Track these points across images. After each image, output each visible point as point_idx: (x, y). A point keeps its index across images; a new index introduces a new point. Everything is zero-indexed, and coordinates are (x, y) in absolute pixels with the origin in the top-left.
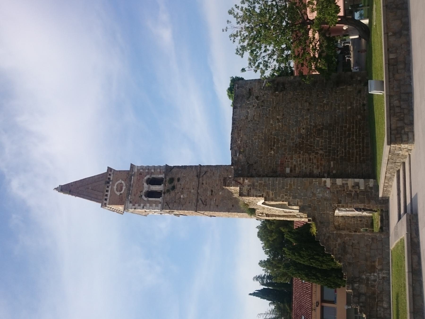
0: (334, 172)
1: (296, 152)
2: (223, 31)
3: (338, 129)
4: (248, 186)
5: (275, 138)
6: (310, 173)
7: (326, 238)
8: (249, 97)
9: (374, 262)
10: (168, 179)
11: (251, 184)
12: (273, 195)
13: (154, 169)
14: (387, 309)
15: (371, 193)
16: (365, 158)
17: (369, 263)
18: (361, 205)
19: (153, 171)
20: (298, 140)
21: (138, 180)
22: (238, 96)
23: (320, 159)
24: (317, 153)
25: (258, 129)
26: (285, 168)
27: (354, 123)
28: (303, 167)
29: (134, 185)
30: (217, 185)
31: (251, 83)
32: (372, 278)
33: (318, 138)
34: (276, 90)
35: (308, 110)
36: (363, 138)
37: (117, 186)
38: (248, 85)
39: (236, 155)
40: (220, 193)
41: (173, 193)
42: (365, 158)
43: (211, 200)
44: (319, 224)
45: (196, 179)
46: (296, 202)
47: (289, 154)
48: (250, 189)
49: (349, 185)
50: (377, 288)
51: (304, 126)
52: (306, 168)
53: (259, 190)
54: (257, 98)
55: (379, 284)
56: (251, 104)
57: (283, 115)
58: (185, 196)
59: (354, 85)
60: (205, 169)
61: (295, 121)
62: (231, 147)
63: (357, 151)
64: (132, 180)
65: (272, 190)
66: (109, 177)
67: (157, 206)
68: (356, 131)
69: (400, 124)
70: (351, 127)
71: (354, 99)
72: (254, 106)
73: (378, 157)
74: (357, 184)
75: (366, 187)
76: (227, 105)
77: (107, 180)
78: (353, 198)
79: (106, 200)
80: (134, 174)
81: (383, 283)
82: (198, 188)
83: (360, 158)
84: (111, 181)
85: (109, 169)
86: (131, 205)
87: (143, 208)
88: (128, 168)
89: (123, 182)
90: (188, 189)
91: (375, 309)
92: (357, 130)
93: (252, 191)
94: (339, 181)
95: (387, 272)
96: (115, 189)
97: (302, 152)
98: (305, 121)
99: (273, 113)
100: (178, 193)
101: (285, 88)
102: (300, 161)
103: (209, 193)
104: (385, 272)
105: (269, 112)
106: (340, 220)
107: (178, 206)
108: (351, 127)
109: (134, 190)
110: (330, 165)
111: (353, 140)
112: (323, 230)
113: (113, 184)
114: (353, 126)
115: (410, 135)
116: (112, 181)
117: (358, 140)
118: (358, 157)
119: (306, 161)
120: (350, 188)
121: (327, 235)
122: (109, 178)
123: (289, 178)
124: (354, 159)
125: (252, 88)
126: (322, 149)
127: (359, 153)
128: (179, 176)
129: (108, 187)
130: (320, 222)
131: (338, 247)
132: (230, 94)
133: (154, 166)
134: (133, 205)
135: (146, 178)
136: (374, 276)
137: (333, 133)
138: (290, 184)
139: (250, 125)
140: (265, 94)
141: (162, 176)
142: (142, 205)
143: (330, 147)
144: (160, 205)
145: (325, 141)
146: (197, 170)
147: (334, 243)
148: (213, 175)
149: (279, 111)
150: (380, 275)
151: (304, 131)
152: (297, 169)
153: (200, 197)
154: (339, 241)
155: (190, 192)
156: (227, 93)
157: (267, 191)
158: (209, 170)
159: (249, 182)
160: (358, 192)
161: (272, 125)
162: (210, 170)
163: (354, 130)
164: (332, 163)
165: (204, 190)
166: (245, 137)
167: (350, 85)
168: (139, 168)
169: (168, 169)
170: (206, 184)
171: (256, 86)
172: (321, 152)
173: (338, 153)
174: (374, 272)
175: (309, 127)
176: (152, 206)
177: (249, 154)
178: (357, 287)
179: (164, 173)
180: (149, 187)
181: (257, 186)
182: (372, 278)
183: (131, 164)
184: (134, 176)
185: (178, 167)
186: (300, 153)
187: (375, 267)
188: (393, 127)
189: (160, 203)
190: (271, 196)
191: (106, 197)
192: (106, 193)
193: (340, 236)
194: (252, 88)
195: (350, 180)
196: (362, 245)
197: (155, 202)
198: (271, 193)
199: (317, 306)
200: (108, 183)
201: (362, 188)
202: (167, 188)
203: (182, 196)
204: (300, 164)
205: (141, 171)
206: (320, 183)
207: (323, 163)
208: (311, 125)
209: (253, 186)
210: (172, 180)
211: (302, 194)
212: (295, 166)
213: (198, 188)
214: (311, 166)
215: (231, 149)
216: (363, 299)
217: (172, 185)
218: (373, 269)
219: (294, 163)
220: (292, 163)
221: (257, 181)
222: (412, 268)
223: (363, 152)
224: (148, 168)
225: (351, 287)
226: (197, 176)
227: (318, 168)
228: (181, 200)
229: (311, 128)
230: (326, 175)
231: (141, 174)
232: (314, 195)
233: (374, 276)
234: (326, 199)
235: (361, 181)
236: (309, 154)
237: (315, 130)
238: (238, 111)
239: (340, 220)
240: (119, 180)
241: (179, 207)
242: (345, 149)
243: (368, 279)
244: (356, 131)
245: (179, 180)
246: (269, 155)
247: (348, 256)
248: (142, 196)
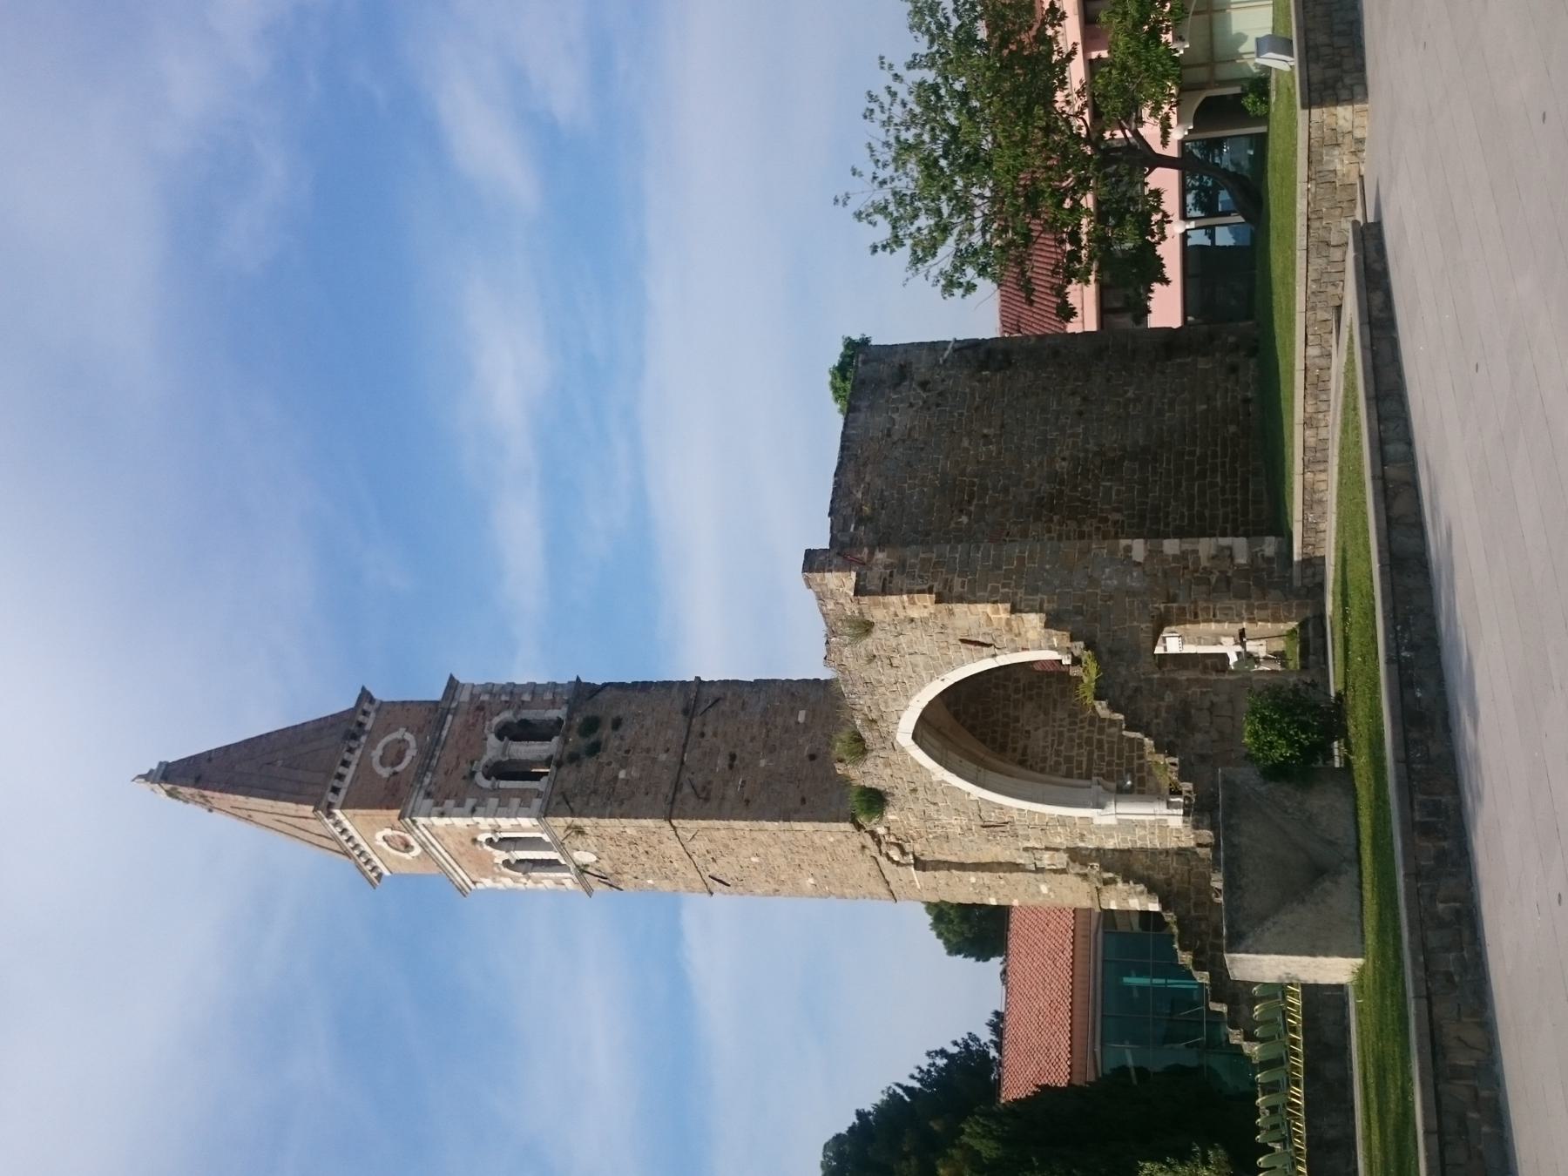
1: (1038, 518)
2: (836, 201)
4: (886, 567)
5: (973, 484)
7: (1128, 692)
8: (898, 384)
10: (578, 720)
15: (1270, 574)
18: (1239, 602)
19: (526, 697)
20: (1046, 487)
21: (469, 727)
22: (863, 382)
24: (1106, 520)
25: (921, 460)
29: (451, 742)
30: (753, 739)
34: (983, 366)
35: (1080, 413)
36: (1245, 482)
37: (384, 748)
39: (845, 529)
40: (763, 763)
41: (589, 766)
43: (726, 783)
44: (1106, 658)
45: (679, 719)
47: (1015, 523)
48: (891, 575)
51: (1067, 453)
54: (924, 385)
56: (902, 401)
57: (1002, 426)
58: (635, 773)
59: (1218, 355)
60: (715, 692)
64: (447, 726)
65: (962, 574)
66: (361, 718)
67: (525, 803)
68: (1223, 464)
69: (1330, 73)
72: (911, 405)
73: (1284, 404)
75: (1253, 557)
76: (824, 425)
77: (353, 728)
78: (1215, 590)
79: (336, 790)
80: (456, 709)
82: (684, 746)
84: (364, 732)
85: (365, 696)
86: (429, 802)
87: (473, 812)
89: (409, 737)
90: (648, 750)
93: (898, 580)
94: (1171, 546)
97: (1056, 518)
98: (1070, 441)
100: (609, 764)
101: (1010, 364)
103: (722, 762)
105: (960, 420)
106: (1173, 863)
107: (605, 805)
111: (1213, 485)
113: (372, 744)
115: (1357, 89)
116: (370, 732)
120: (1204, 563)
121: (1132, 684)
122: (361, 725)
126: (1118, 510)
128: (615, 713)
129: (351, 750)
130: (1110, 651)
131: (1164, 714)
132: (839, 384)
133: (535, 684)
134: (436, 804)
135: (496, 720)
137: (1154, 468)
139: (898, 452)
140: (950, 377)
142: (470, 802)
144: (537, 802)
147: (1154, 705)
148: (743, 708)
151: (1064, 464)
153: (686, 775)
154: (1169, 697)
155: (654, 760)
156: (829, 378)
158: (729, 694)
161: (967, 450)
165: (705, 754)
166: (879, 482)
168: (476, 691)
169: (583, 692)
170: (715, 734)
175: (1081, 455)
176: (506, 805)
179: (567, 702)
180: (505, 748)
181: (913, 566)
184: (454, 715)
185: (621, 686)
186: (1051, 520)
188: (1314, 79)
189: (539, 794)
190: (957, 589)
191: (336, 783)
192: (341, 770)
193: (1171, 684)
197: (521, 793)
198: (957, 581)
200: (355, 737)
201: (1242, 560)
202: (569, 749)
203: (622, 775)
205: (485, 697)
206: (1112, 553)
208: (1086, 451)
209: (902, 566)
210: (591, 725)
211: (1057, 582)
213: (684, 746)
217: (593, 739)
221: (914, 555)
222: (1370, 316)
225: (1206, 822)
226: (685, 712)
229: (1086, 459)
231: (480, 708)
232: (1093, 582)
234: (1131, 593)
235: (1240, 544)
236: (1080, 523)
238: (861, 417)
239: (1173, 863)
241: (609, 809)
242: (1191, 508)
244: (1223, 464)
245: (617, 724)
246: (953, 525)
247: (1199, 737)
248: (473, 774)
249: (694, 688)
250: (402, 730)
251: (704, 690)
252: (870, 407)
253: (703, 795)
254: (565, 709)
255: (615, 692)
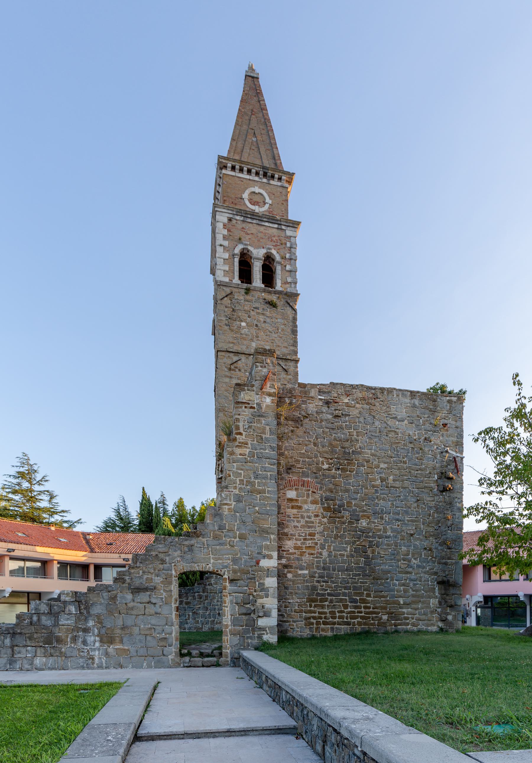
0: (290, 576)
3: (366, 583)
6: (286, 534)
7: (161, 556)
9: (121, 642)
11: (263, 410)
12: (241, 455)
13: (291, 271)
14: (32, 664)
15: (251, 638)
16: (315, 626)
17: (118, 631)
19: (288, 268)
21: (270, 238)
23: (313, 552)
24: (323, 548)
26: (296, 489)
27: (373, 609)
28: (298, 522)
29: (262, 229)
31: (457, 427)
32: (90, 639)
33: (351, 550)
38: (454, 423)
39: (320, 392)
42: (315, 626)
46: (228, 502)
49: (265, 599)
50: (71, 647)
52: (295, 527)
53: (250, 427)
55: (79, 650)
59: (439, 610)
60: (291, 369)
61: (382, 510)
62: (337, 384)
63: (325, 613)
64: (271, 225)
65: (252, 455)
70: (368, 605)
71: (416, 609)
74: (267, 614)
75: (263, 629)
81: (82, 657)
83: (314, 618)
84: (269, 180)
88: (291, 217)
89: (267, 207)
90: (257, 337)
91: (29, 643)
92: (363, 614)
94: (271, 582)
95: (104, 665)
96: (252, 189)
97: (325, 520)
98: (381, 527)
99: (399, 469)
102: (309, 517)
104: (104, 661)
108: (368, 605)
109: (252, 227)
110: (302, 569)
111: (346, 607)
112: (176, 551)
113: (262, 186)
114: (369, 608)
117: (344, 614)
118: (317, 615)
119: (309, 527)
120: (260, 601)
122: (273, 177)
123: (276, 489)
124: (312, 609)
125: (447, 430)
126: (329, 556)
127: (323, 616)
129: (257, 174)
135: (274, 252)
136: (95, 641)
137: (359, 575)
138: (264, 492)
141: (279, 286)
143: (334, 570)
145: (343, 562)
146: (290, 354)
149: (403, 481)
150: (97, 653)
152: (295, 511)
153: (243, 357)
154: (158, 580)
155: (252, 340)
157: (249, 442)
158: (289, 377)
159: (267, 406)
160: (252, 615)
162: (290, 379)
163: (363, 610)
164: (306, 572)
167: (440, 603)
171: (451, 439)
172: (325, 553)
173: (323, 582)
174: (101, 641)
177: (322, 421)
178: (69, 610)
181: (259, 422)
182: (90, 639)
183: (298, 223)
185: (295, 319)
187: (112, 643)
194: (447, 430)
195: (276, 601)
196: (154, 621)
199: (124, 559)
200: (265, 175)
203: (243, 324)
204: (303, 517)
206: (267, 548)
207: (306, 558)
212: (300, 508)
214: (300, 536)
215: (332, 384)
216: (46, 621)
218: (107, 639)
219: (305, 507)
220: (306, 502)
223: (325, 623)
224: (293, 259)
227: (296, 548)
228: (238, 323)
230: (284, 561)
233: (95, 641)
236: (322, 533)
237: (363, 544)
238: (407, 400)
240: (270, 199)
242: (329, 595)
243: (86, 630)
244: (361, 612)
246: (321, 459)
247: (129, 596)
249: (294, 357)
250: (270, 202)
251: (292, 364)
252: (414, 406)
253: (232, 367)
254: (281, 289)
255: (291, 317)
